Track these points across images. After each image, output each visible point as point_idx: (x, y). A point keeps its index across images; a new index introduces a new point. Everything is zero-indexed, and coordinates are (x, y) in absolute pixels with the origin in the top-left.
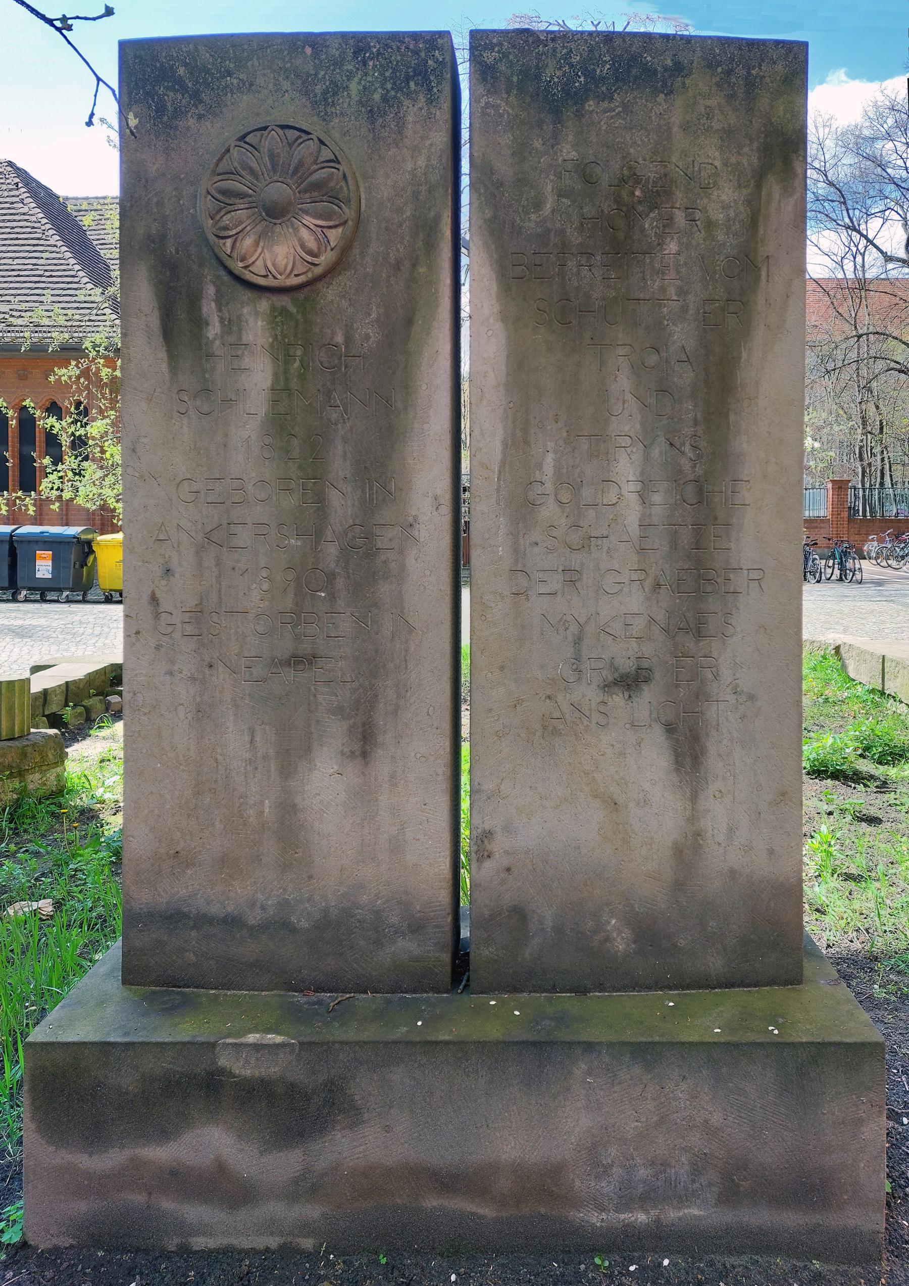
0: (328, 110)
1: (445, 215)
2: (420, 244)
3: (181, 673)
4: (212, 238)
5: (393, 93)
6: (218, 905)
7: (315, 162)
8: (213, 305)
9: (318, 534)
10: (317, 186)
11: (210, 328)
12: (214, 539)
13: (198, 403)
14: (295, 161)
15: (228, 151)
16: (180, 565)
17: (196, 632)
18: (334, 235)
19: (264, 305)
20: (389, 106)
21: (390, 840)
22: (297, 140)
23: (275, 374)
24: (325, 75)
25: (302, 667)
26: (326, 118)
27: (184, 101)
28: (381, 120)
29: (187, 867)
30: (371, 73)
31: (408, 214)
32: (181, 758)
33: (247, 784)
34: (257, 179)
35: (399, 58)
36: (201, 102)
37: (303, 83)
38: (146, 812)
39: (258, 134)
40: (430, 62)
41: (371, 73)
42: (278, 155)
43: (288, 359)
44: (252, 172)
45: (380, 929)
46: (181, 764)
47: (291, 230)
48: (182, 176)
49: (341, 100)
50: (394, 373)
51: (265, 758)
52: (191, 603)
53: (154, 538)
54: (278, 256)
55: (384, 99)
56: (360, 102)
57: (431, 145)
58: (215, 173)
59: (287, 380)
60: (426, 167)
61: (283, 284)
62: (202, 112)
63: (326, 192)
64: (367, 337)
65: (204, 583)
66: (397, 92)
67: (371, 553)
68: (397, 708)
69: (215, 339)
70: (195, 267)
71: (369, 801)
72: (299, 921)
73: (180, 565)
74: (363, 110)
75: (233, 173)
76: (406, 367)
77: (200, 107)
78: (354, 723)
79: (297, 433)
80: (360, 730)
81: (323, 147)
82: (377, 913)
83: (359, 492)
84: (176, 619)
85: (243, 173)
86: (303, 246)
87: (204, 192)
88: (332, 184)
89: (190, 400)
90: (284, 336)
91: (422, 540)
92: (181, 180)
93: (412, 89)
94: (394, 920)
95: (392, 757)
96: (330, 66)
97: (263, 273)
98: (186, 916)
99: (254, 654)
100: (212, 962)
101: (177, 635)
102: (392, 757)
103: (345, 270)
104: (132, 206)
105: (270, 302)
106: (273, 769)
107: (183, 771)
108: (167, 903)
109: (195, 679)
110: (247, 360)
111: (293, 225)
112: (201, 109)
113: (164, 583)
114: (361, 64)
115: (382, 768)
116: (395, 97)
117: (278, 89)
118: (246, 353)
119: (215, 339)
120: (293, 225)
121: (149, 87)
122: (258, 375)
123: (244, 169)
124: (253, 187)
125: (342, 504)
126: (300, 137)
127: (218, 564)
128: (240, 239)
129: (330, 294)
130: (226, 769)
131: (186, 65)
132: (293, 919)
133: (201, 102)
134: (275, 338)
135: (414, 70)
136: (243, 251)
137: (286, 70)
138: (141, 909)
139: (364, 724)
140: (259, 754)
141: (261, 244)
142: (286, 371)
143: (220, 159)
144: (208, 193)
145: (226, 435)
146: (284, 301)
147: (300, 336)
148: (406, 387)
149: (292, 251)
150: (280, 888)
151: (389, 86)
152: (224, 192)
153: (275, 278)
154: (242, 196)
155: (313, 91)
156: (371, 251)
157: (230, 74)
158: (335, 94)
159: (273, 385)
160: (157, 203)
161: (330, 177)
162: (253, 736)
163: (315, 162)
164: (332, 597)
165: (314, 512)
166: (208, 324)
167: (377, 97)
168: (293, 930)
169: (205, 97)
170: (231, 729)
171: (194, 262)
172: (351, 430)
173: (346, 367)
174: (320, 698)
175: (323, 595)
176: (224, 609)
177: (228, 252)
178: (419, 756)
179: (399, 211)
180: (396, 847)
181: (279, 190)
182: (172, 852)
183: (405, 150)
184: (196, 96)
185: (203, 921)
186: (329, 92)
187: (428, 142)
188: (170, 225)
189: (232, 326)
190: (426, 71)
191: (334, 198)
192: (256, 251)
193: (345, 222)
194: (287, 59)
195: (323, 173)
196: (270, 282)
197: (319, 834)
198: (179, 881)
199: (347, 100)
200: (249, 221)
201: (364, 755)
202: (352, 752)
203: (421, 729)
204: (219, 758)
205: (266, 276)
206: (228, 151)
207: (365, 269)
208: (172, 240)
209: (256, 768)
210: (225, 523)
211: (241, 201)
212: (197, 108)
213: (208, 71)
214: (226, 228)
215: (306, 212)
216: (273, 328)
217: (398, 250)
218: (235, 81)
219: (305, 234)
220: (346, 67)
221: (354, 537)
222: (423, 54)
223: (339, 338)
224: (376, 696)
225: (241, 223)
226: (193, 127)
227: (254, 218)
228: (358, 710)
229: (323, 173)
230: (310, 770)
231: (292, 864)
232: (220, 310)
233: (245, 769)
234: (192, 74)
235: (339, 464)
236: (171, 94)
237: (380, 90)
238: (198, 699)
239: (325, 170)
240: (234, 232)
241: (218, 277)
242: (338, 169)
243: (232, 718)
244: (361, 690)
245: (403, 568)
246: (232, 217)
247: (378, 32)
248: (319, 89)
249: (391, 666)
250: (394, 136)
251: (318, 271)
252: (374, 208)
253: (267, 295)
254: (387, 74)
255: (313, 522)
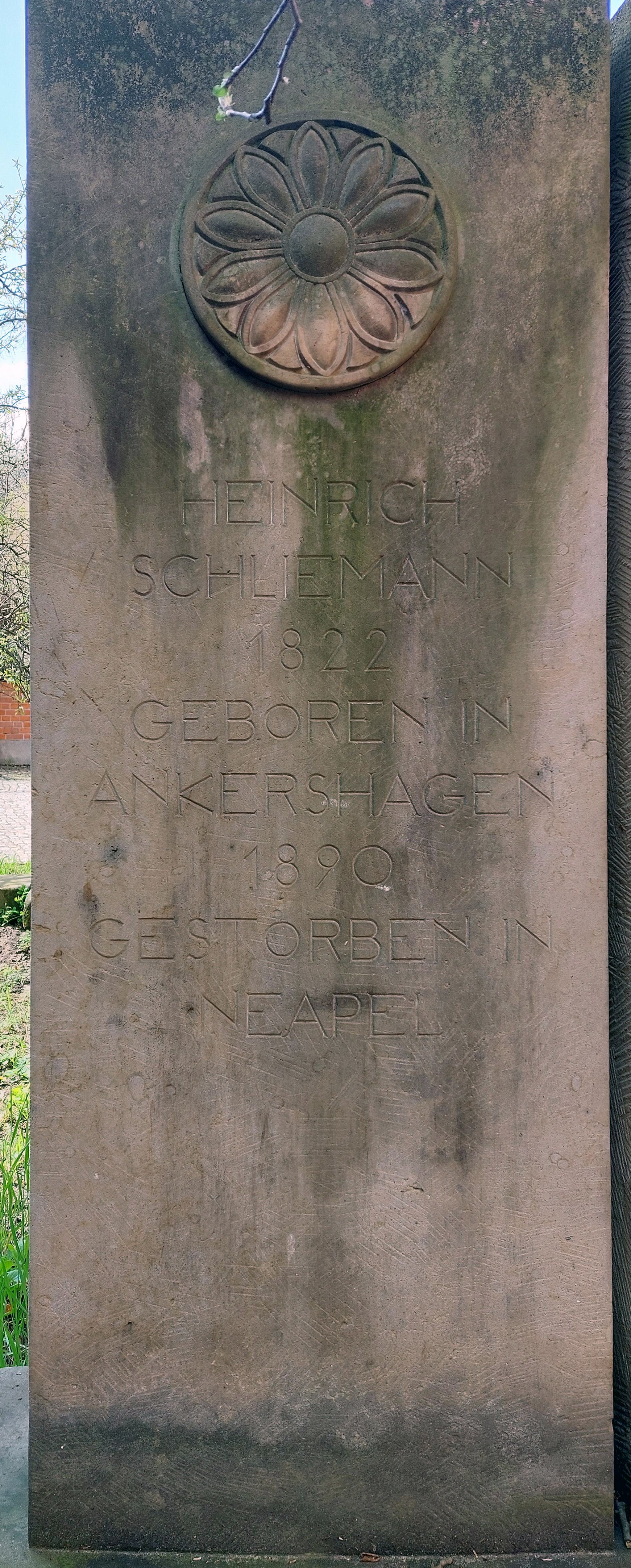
0: (403, 98)
1: (601, 272)
2: (558, 319)
3: (135, 1020)
4: (201, 305)
5: (513, 74)
6: (204, 1411)
7: (384, 184)
8: (198, 416)
9: (377, 791)
10: (391, 221)
11: (193, 453)
12: (198, 799)
13: (171, 576)
14: (352, 180)
15: (231, 160)
16: (136, 840)
17: (165, 952)
18: (420, 304)
19: (288, 416)
20: (507, 95)
21: (509, 1299)
22: (353, 145)
23: (307, 531)
24: (396, 41)
25: (350, 1010)
26: (397, 112)
27: (146, 78)
28: (493, 117)
29: (148, 1347)
30: (476, 41)
31: (539, 269)
32: (137, 1164)
33: (255, 1207)
34: (284, 209)
35: (524, 17)
36: (177, 80)
37: (359, 54)
38: (73, 1255)
39: (286, 134)
40: (577, 25)
41: (476, 41)
42: (322, 170)
43: (330, 504)
44: (276, 196)
45: (492, 1447)
46: (136, 1175)
47: (343, 294)
48: (143, 202)
49: (424, 83)
50: (511, 528)
51: (288, 1162)
52: (157, 903)
53: (90, 797)
54: (320, 335)
55: (499, 83)
56: (457, 87)
57: (578, 159)
58: (205, 197)
59: (326, 539)
60: (569, 194)
61: (328, 383)
62: (179, 97)
63: (411, 237)
64: (466, 470)
65: (181, 870)
66: (520, 73)
67: (469, 820)
68: (516, 1079)
69: (202, 472)
70: (165, 352)
71: (471, 1234)
72: (350, 1436)
73: (136, 840)
74: (463, 99)
75: (241, 198)
76: (532, 518)
77: (175, 88)
78: (444, 1104)
79: (347, 629)
80: (454, 1114)
81: (400, 158)
82: (487, 1421)
83: (449, 721)
84: (129, 932)
85: (259, 198)
86: (365, 321)
87: (189, 228)
88: (416, 220)
89: (156, 571)
90: (323, 468)
91: (556, 798)
92: (141, 208)
93: (547, 68)
94: (517, 1431)
95: (510, 1160)
96: (405, 27)
97: (295, 363)
98: (148, 1431)
99: (267, 988)
100: (195, 1508)
101: (130, 957)
102: (510, 1160)
103: (429, 360)
104: (51, 249)
105: (299, 412)
106: (301, 1182)
107: (141, 1186)
108: (111, 1409)
109: (161, 1031)
110: (257, 507)
111: (347, 287)
112: (177, 92)
113: (107, 871)
114: (459, 25)
115: (492, 1176)
116: (517, 80)
117: (315, 63)
118: (256, 496)
119: (202, 472)
120: (347, 287)
121: (83, 53)
122: (276, 533)
123: (260, 191)
124: (277, 222)
125: (419, 743)
126: (359, 141)
127: (204, 840)
128: (253, 307)
129: (404, 399)
130: (218, 1183)
131: (150, 18)
132: (340, 1434)
133: (177, 80)
134: (308, 469)
135: (550, 38)
136: (261, 328)
137: (329, 32)
138: (63, 1418)
139: (460, 1105)
140: (277, 1157)
141: (291, 316)
142: (325, 525)
143: (218, 175)
144: (197, 230)
145: (220, 630)
146: (325, 410)
147: (350, 467)
148: (533, 550)
149: (346, 327)
150: (316, 1383)
151: (507, 62)
152: (226, 230)
153: (313, 372)
154: (257, 235)
155: (375, 67)
156: (474, 329)
157: (229, 35)
158: (414, 72)
159: (302, 548)
160: (97, 246)
161: (414, 208)
162: (266, 1126)
163: (384, 184)
164: (403, 892)
165: (372, 753)
166: (188, 447)
167: (486, 79)
168: (340, 1452)
169: (186, 71)
170: (226, 1115)
171: (165, 345)
172: (437, 619)
173: (429, 517)
174: (383, 1061)
175: (387, 889)
176: (214, 914)
177: (233, 329)
178: (556, 1157)
179: (523, 264)
180: (519, 1309)
181: (318, 228)
182: (122, 1322)
183: (534, 166)
184: (168, 72)
185: (176, 1438)
186: (403, 70)
187: (573, 155)
188: (120, 282)
189: (231, 450)
190: (571, 40)
191: (419, 243)
192: (281, 327)
193: (438, 282)
194: (330, 14)
195: (403, 201)
196: (304, 379)
197: (384, 1290)
198: (133, 1371)
199: (435, 83)
200: (270, 278)
201: (461, 1156)
202: (441, 1153)
203: (560, 1113)
204: (206, 1163)
205: (296, 370)
206: (231, 160)
207: (464, 358)
208: (124, 308)
209: (272, 1181)
210: (217, 772)
211: (256, 244)
212: (170, 90)
213: (189, 30)
214: (229, 289)
215: (371, 265)
216: (303, 455)
217: (520, 330)
218: (239, 48)
219: (369, 300)
220: (432, 30)
221: (441, 794)
222: (565, 12)
223: (418, 472)
224: (480, 1058)
225: (256, 280)
226: (162, 121)
227: (278, 272)
228: (449, 1081)
229: (403, 201)
230: (368, 1183)
231: (336, 1342)
232: (210, 425)
233: (253, 1182)
234: (160, 32)
235: (415, 675)
236: (124, 66)
237: (491, 69)
238: (168, 1065)
239: (404, 195)
240: (243, 295)
241: (207, 370)
242: (427, 195)
243: (228, 1096)
244: (454, 1048)
245: (524, 844)
246: (242, 271)
247: (27, 17)
248: (386, 63)
249: (504, 1006)
250: (516, 144)
251: (389, 361)
252: (481, 260)
253: (294, 400)
254: (504, 43)
255: (370, 773)
